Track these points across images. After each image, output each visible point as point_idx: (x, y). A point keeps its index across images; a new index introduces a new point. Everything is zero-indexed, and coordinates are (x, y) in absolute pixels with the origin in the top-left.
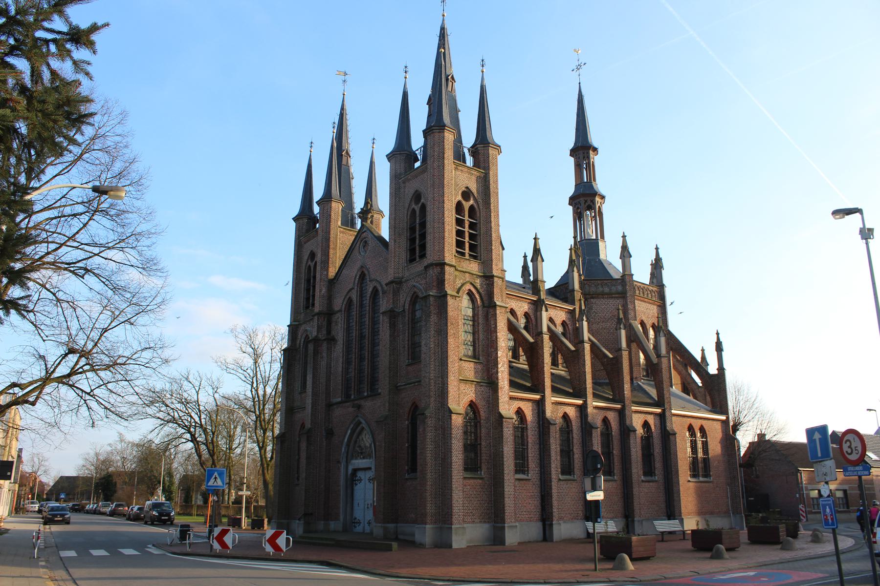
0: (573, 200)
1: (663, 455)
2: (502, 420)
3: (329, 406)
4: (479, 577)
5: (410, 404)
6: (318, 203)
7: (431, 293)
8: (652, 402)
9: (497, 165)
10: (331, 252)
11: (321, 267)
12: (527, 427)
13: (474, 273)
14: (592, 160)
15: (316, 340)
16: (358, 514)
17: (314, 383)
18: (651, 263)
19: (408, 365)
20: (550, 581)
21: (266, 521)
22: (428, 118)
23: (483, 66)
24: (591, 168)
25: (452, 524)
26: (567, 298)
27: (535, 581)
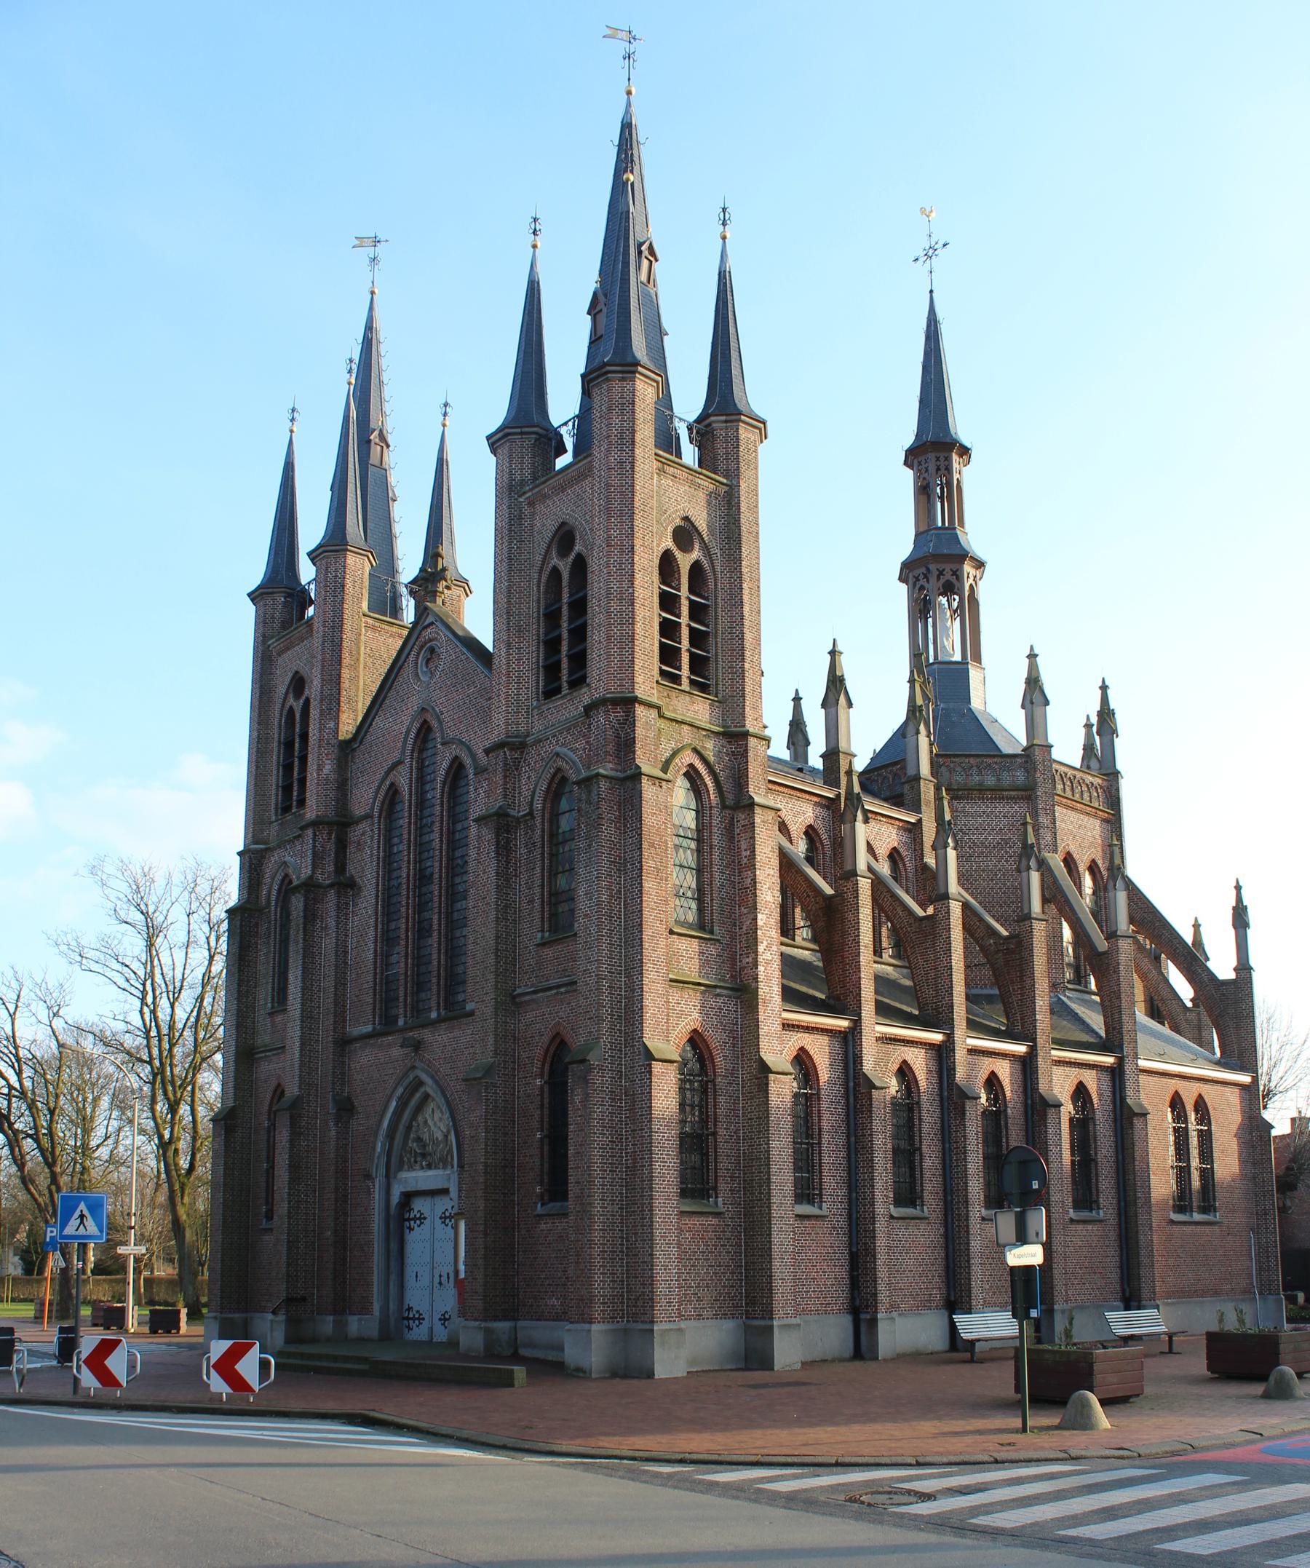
0: (909, 571)
1: (1117, 1162)
2: (767, 1078)
3: (344, 1044)
4: (754, 1451)
5: (546, 1039)
6: (313, 556)
7: (601, 771)
8: (1092, 1040)
9: (756, 468)
10: (346, 674)
11: (322, 711)
12: (818, 1094)
13: (703, 725)
14: (956, 476)
15: (310, 886)
16: (417, 1297)
17: (305, 989)
18: (1084, 722)
19: (542, 945)
20: (929, 1459)
21: (184, 1312)
22: (589, 348)
23: (724, 224)
24: (952, 494)
25: (652, 1322)
26: (901, 795)
27: (894, 1460)
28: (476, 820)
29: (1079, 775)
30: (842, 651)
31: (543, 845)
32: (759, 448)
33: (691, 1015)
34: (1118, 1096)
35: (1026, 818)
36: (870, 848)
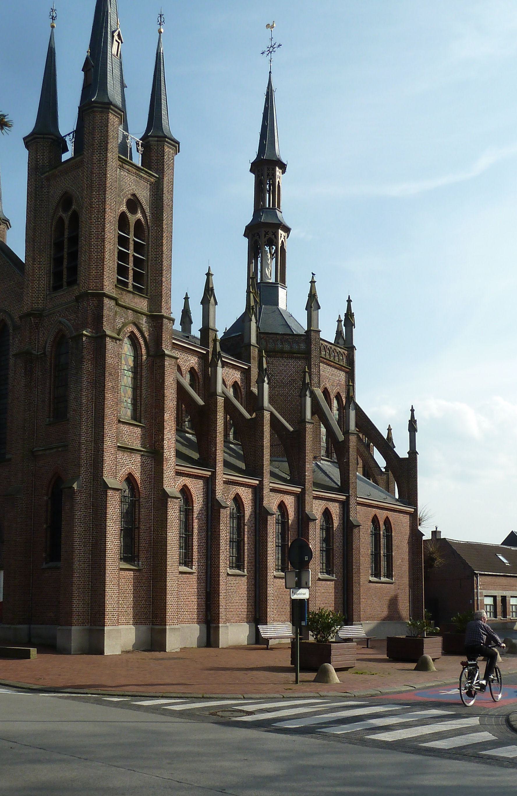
7: (84, 332)
9: (173, 169)
24: (275, 190)
28: (14, 355)
29: (333, 347)
30: (213, 273)
31: (51, 371)
32: (175, 157)
33: (128, 466)
34: (346, 515)
35: (305, 369)
36: (224, 382)
